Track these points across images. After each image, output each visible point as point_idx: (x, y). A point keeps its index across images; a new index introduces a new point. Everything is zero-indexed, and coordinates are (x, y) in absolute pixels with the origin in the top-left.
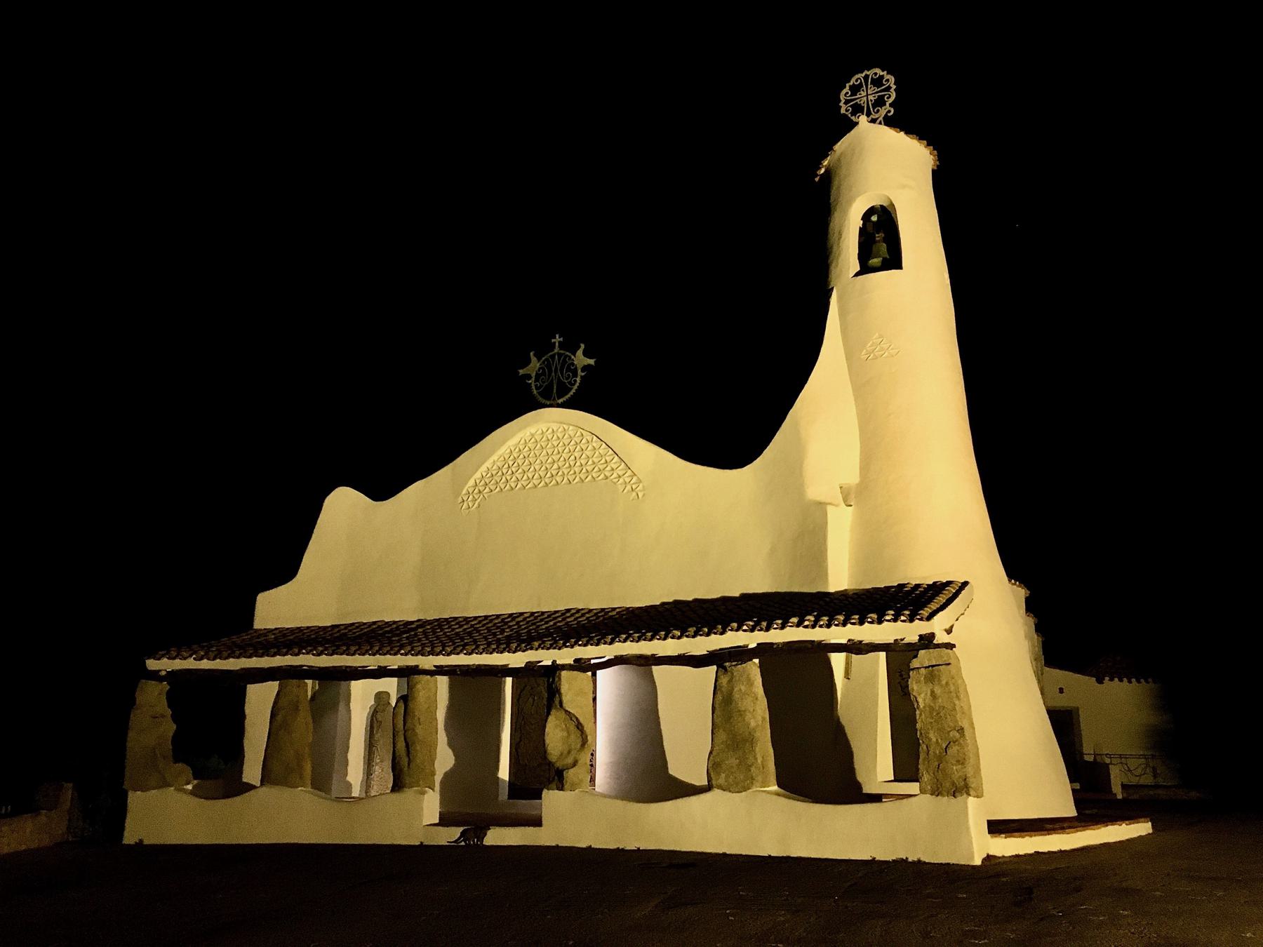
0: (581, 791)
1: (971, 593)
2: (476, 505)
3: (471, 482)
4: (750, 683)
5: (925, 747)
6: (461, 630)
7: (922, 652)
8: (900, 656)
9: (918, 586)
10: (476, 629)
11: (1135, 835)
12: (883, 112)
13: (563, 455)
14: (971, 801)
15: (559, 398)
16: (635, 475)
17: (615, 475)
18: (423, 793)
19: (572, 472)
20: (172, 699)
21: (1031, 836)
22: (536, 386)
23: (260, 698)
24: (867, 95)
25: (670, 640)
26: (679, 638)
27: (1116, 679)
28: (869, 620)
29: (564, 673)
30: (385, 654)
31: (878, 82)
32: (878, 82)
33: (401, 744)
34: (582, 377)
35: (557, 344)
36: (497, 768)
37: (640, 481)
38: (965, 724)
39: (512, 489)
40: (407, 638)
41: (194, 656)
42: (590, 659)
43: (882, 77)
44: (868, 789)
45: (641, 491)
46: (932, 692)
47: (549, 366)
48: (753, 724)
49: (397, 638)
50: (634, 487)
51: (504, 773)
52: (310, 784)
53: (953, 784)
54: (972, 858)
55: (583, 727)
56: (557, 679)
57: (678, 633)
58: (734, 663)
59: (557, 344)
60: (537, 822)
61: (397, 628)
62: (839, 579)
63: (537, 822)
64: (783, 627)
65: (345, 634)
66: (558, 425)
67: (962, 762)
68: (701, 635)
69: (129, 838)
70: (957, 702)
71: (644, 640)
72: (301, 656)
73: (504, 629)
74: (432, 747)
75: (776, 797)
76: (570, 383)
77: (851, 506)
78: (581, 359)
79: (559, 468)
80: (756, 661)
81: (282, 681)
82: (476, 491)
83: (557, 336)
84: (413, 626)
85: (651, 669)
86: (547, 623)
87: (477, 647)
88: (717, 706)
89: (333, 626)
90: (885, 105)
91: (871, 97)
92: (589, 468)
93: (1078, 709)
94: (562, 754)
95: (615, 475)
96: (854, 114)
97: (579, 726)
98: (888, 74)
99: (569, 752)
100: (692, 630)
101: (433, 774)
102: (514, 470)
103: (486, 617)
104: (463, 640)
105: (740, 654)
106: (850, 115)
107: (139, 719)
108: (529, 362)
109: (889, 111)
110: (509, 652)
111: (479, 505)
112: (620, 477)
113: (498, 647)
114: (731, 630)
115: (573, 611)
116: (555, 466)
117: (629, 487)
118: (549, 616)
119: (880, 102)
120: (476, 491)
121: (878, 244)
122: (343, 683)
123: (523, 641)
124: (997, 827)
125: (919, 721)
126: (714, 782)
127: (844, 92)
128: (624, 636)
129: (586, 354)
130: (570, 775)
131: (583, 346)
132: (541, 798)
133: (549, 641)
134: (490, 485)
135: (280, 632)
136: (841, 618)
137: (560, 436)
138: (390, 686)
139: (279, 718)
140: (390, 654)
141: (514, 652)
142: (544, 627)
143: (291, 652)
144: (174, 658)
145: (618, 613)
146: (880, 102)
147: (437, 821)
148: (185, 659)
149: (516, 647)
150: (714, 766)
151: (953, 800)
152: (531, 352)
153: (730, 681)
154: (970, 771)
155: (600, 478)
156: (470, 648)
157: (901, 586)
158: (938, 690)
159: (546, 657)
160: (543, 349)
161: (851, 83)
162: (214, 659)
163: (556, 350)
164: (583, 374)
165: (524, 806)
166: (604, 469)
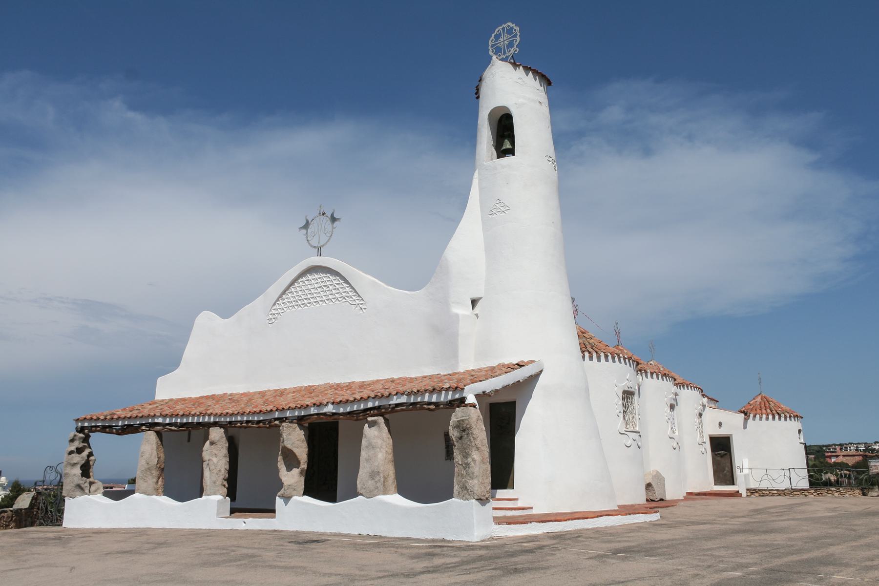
31: (510, 31)
32: (510, 31)
43: (512, 28)
93: (731, 435)
98: (515, 26)
109: (516, 51)
146: (510, 45)
161: (495, 34)
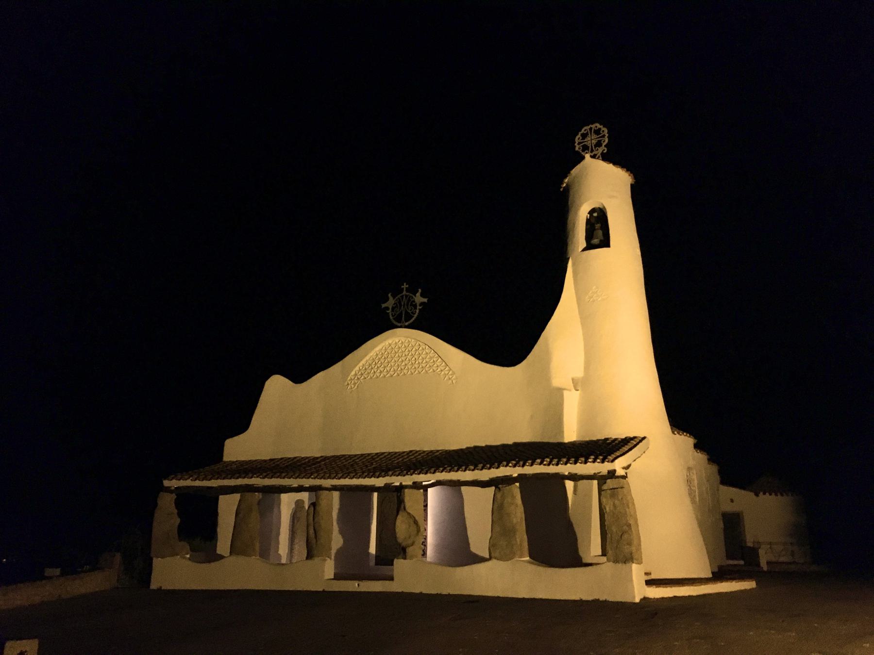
0: (417, 560)
1: (648, 443)
2: (356, 387)
3: (353, 373)
4: (513, 497)
5: (610, 535)
6: (347, 463)
7: (608, 481)
8: (602, 479)
9: (616, 439)
10: (356, 462)
11: (743, 588)
12: (600, 150)
13: (408, 357)
14: (634, 566)
15: (406, 322)
16: (451, 370)
17: (439, 370)
18: (325, 560)
19: (413, 367)
20: (177, 503)
21: (671, 587)
22: (392, 314)
23: (228, 505)
24: (591, 140)
25: (467, 472)
26: (473, 470)
27: (773, 494)
28: (580, 461)
29: (406, 490)
30: (302, 478)
31: (597, 132)
32: (597, 132)
33: (312, 531)
34: (419, 309)
35: (405, 289)
36: (368, 547)
37: (454, 373)
38: (631, 522)
39: (420, 373)
40: (315, 468)
41: (191, 478)
42: (422, 482)
43: (600, 129)
44: (586, 560)
45: (454, 379)
46: (614, 504)
47: (400, 303)
48: (515, 521)
49: (309, 468)
50: (450, 377)
51: (373, 549)
52: (258, 554)
53: (624, 556)
54: (634, 597)
55: (417, 522)
56: (402, 494)
57: (472, 467)
58: (504, 486)
59: (405, 289)
60: (391, 579)
61: (309, 462)
62: (571, 434)
63: (391, 579)
64: (532, 465)
65: (278, 465)
66: (406, 339)
67: (630, 544)
68: (485, 469)
69: (154, 586)
70: (627, 510)
71: (453, 471)
72: (253, 479)
73: (372, 463)
74: (330, 532)
75: (529, 564)
76: (412, 313)
77: (578, 390)
78: (419, 299)
79: (406, 365)
80: (518, 484)
81: (242, 493)
82: (356, 378)
83: (405, 284)
84: (319, 460)
85: (460, 488)
86: (398, 459)
87: (356, 474)
88: (494, 510)
89: (270, 459)
90: (602, 146)
91: (593, 141)
92: (424, 365)
94: (405, 538)
95: (439, 370)
96: (583, 151)
97: (416, 522)
99: (410, 537)
100: (480, 466)
101: (330, 549)
102: (379, 365)
103: (362, 455)
104: (348, 469)
105: (508, 480)
106: (581, 152)
107: (159, 515)
108: (387, 300)
109: (604, 150)
110: (374, 477)
111: (358, 386)
112: (442, 371)
113: (368, 474)
114: (503, 466)
115: (386, 454)
116: (403, 364)
117: (447, 377)
118: (399, 455)
119: (599, 144)
120: (356, 378)
121: (597, 231)
122: (276, 495)
123: (383, 471)
124: (650, 583)
125: (607, 521)
126: (493, 555)
127: (577, 137)
128: (441, 469)
129: (422, 295)
130: (409, 550)
131: (420, 290)
132: (392, 564)
133: (398, 471)
134: (364, 375)
135: (239, 463)
136: (565, 460)
137: (407, 345)
138: (305, 496)
139: (241, 515)
140: (306, 478)
141: (378, 477)
142: (396, 462)
143: (247, 476)
144: (179, 480)
145: (440, 454)
146: (599, 144)
147: (333, 577)
148: (186, 480)
149: (379, 475)
150: (492, 546)
151: (624, 565)
152: (388, 293)
153: (501, 497)
154: (634, 549)
155: (430, 371)
156: (352, 475)
157: (606, 439)
158: (616, 502)
159: (396, 481)
160: (397, 292)
162: (203, 480)
163: (404, 293)
164: (421, 307)
165: (384, 569)
166: (433, 366)
